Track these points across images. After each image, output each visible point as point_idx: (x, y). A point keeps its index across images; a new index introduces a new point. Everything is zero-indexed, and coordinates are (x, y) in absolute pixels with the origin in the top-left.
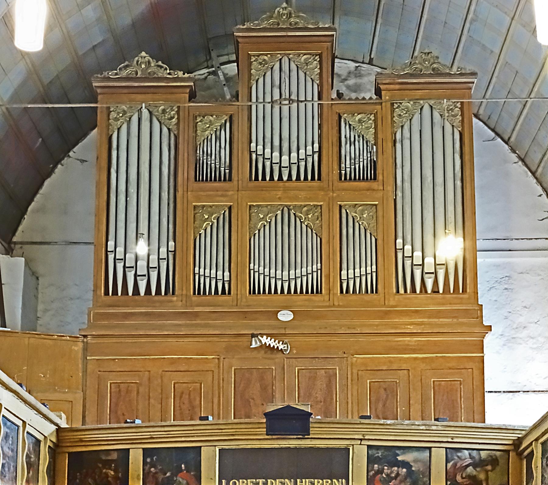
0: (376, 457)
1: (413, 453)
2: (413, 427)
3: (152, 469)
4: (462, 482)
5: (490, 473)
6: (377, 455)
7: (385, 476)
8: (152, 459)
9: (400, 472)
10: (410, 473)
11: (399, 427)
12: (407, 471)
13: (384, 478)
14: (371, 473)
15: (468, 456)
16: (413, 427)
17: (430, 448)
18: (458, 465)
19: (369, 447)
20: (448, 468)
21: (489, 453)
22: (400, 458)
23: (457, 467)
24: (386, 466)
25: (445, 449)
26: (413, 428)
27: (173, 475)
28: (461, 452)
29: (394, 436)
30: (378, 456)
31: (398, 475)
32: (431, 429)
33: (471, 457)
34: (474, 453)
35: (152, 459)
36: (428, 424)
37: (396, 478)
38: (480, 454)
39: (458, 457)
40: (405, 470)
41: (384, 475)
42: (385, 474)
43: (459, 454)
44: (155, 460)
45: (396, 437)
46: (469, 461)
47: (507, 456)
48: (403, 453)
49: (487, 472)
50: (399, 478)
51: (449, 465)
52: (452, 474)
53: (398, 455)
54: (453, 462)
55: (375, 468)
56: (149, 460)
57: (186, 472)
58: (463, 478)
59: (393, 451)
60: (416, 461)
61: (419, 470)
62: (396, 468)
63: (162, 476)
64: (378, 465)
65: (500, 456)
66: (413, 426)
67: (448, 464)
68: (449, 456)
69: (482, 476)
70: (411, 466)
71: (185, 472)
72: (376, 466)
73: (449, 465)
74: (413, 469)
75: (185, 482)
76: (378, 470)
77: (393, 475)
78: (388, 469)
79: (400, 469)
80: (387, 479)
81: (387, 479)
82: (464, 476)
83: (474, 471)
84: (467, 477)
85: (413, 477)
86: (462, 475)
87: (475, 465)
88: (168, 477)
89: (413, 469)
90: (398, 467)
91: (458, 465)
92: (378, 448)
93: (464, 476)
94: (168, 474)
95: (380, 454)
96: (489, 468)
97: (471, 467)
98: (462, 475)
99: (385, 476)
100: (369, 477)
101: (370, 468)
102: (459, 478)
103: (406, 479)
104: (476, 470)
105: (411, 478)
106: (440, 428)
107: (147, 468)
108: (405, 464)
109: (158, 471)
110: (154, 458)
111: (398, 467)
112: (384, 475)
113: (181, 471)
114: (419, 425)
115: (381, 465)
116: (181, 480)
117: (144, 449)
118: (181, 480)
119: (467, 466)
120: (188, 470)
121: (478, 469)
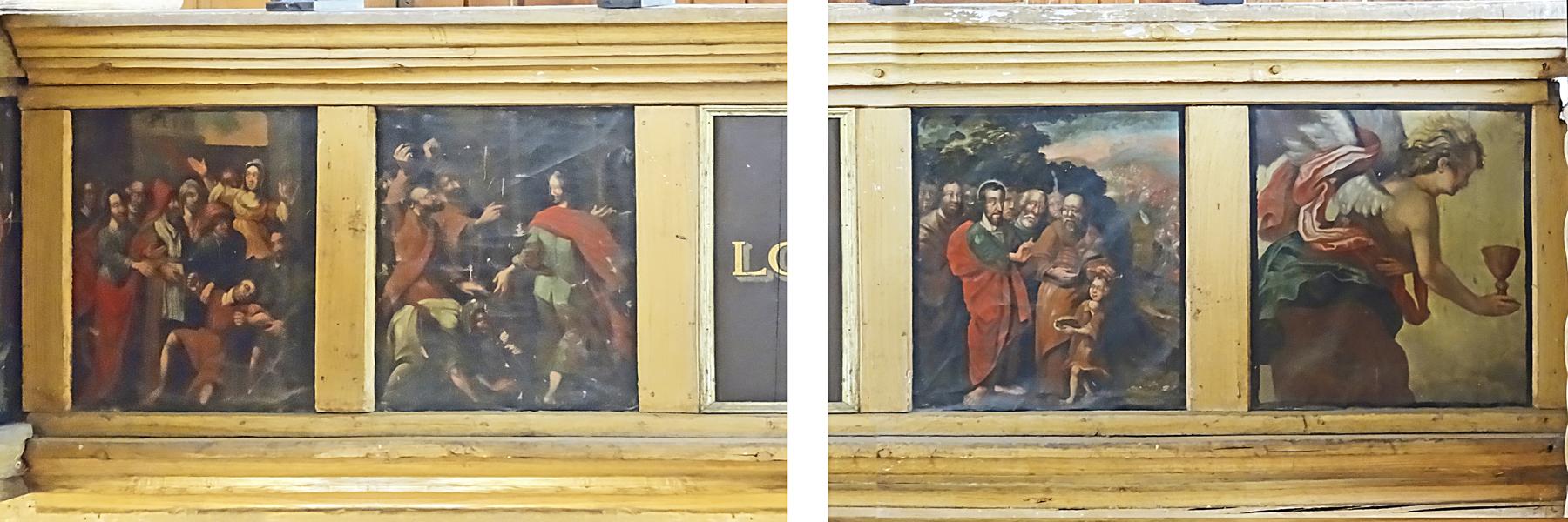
0: (949, 153)
1: (1112, 132)
2: (1093, 31)
3: (420, 193)
4: (1321, 241)
5: (1442, 199)
6: (955, 144)
7: (989, 227)
8: (417, 153)
9: (1053, 210)
10: (1098, 208)
11: (1031, 32)
12: (1084, 203)
13: (988, 234)
14: (930, 220)
15: (1347, 134)
16: (1093, 31)
17: (1181, 109)
18: (1306, 173)
19: (918, 112)
20: (1262, 185)
21: (1442, 120)
22: (1051, 153)
23: (1299, 182)
24: (996, 187)
25: (1247, 108)
26: (1094, 37)
27: (507, 217)
28: (1318, 119)
29: (1017, 70)
30: (960, 150)
31: (1044, 220)
32: (1174, 35)
33: (1362, 139)
34: (1374, 122)
35: (417, 153)
36: (1155, 17)
37: (1036, 231)
38: (1399, 122)
39: (1304, 139)
40: (1073, 200)
41: (985, 223)
42: (990, 219)
43: (1308, 129)
44: (428, 154)
45: (1027, 70)
46: (1350, 154)
47: (1522, 128)
48: (1064, 134)
49: (1432, 195)
50: (1048, 233)
51: (1265, 175)
52: (1278, 212)
53: (1045, 141)
54: (1282, 160)
55: (947, 198)
56: (402, 154)
57: (569, 206)
58: (1325, 224)
59: (1024, 125)
60: (1121, 163)
61: (1134, 196)
62: (1037, 195)
63: (465, 222)
64: (960, 184)
65: (1493, 127)
66: (1093, 28)
67: (1261, 169)
68: (1263, 132)
69: (1410, 215)
70: (1102, 184)
71: (564, 205)
72: (952, 187)
73: (1265, 175)
74: (1110, 194)
75: (563, 245)
76: (960, 205)
77: (1025, 222)
78: (1002, 199)
79: (1055, 196)
80: (999, 236)
81: (999, 236)
82: (1330, 216)
83: (1376, 192)
84: (1346, 220)
85: (1111, 228)
86: (1321, 211)
87: (1379, 171)
88: (489, 225)
89: (1110, 194)
90: (1047, 190)
91: (1306, 173)
92: (959, 115)
93: (1330, 216)
94: (490, 213)
95: (968, 140)
96: (1442, 179)
97: (1361, 179)
98: (1321, 211)
99: (989, 227)
100: (922, 233)
101: (925, 198)
102: (1307, 224)
103: (1079, 233)
104: (1385, 191)
105: (1100, 228)
106: (1214, 30)
107: (395, 186)
108: (1074, 176)
109: (444, 199)
110: (426, 147)
111: (1047, 190)
112: (985, 223)
113: (547, 202)
114: (1117, 24)
115: (975, 185)
116: (546, 237)
117: (379, 110)
118: (546, 237)
119: (1346, 175)
120: (577, 195)
121: (1391, 187)
